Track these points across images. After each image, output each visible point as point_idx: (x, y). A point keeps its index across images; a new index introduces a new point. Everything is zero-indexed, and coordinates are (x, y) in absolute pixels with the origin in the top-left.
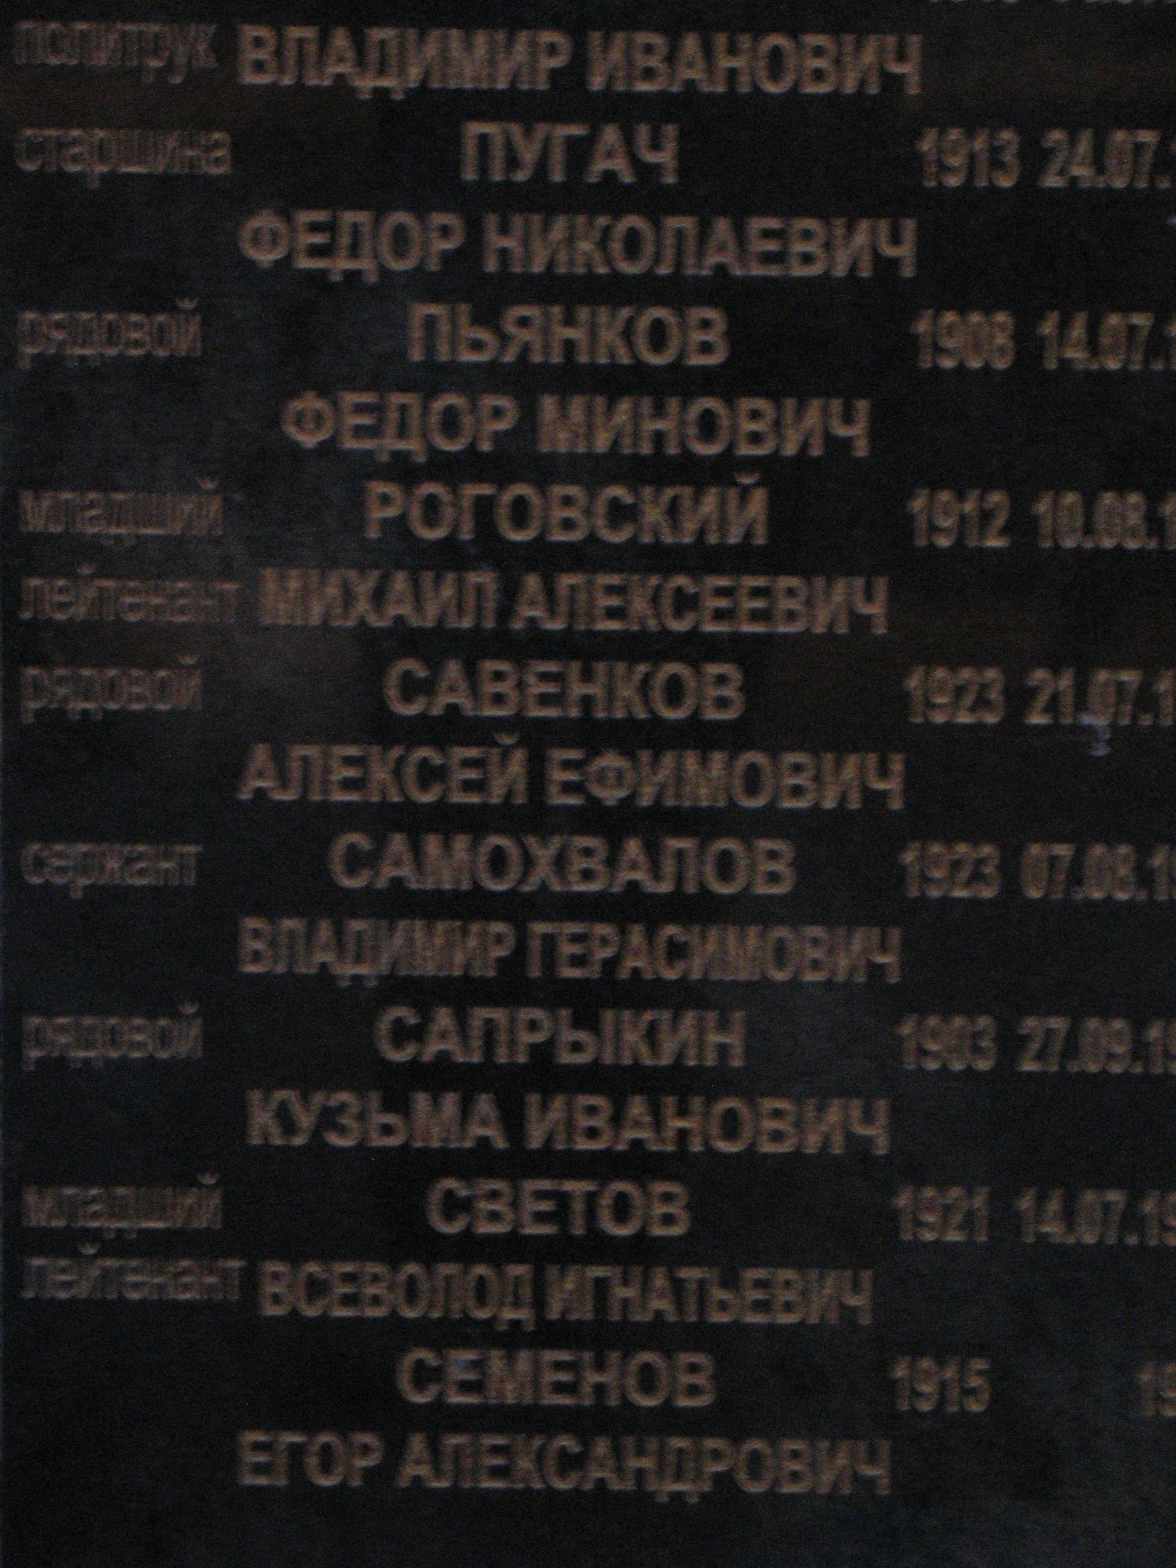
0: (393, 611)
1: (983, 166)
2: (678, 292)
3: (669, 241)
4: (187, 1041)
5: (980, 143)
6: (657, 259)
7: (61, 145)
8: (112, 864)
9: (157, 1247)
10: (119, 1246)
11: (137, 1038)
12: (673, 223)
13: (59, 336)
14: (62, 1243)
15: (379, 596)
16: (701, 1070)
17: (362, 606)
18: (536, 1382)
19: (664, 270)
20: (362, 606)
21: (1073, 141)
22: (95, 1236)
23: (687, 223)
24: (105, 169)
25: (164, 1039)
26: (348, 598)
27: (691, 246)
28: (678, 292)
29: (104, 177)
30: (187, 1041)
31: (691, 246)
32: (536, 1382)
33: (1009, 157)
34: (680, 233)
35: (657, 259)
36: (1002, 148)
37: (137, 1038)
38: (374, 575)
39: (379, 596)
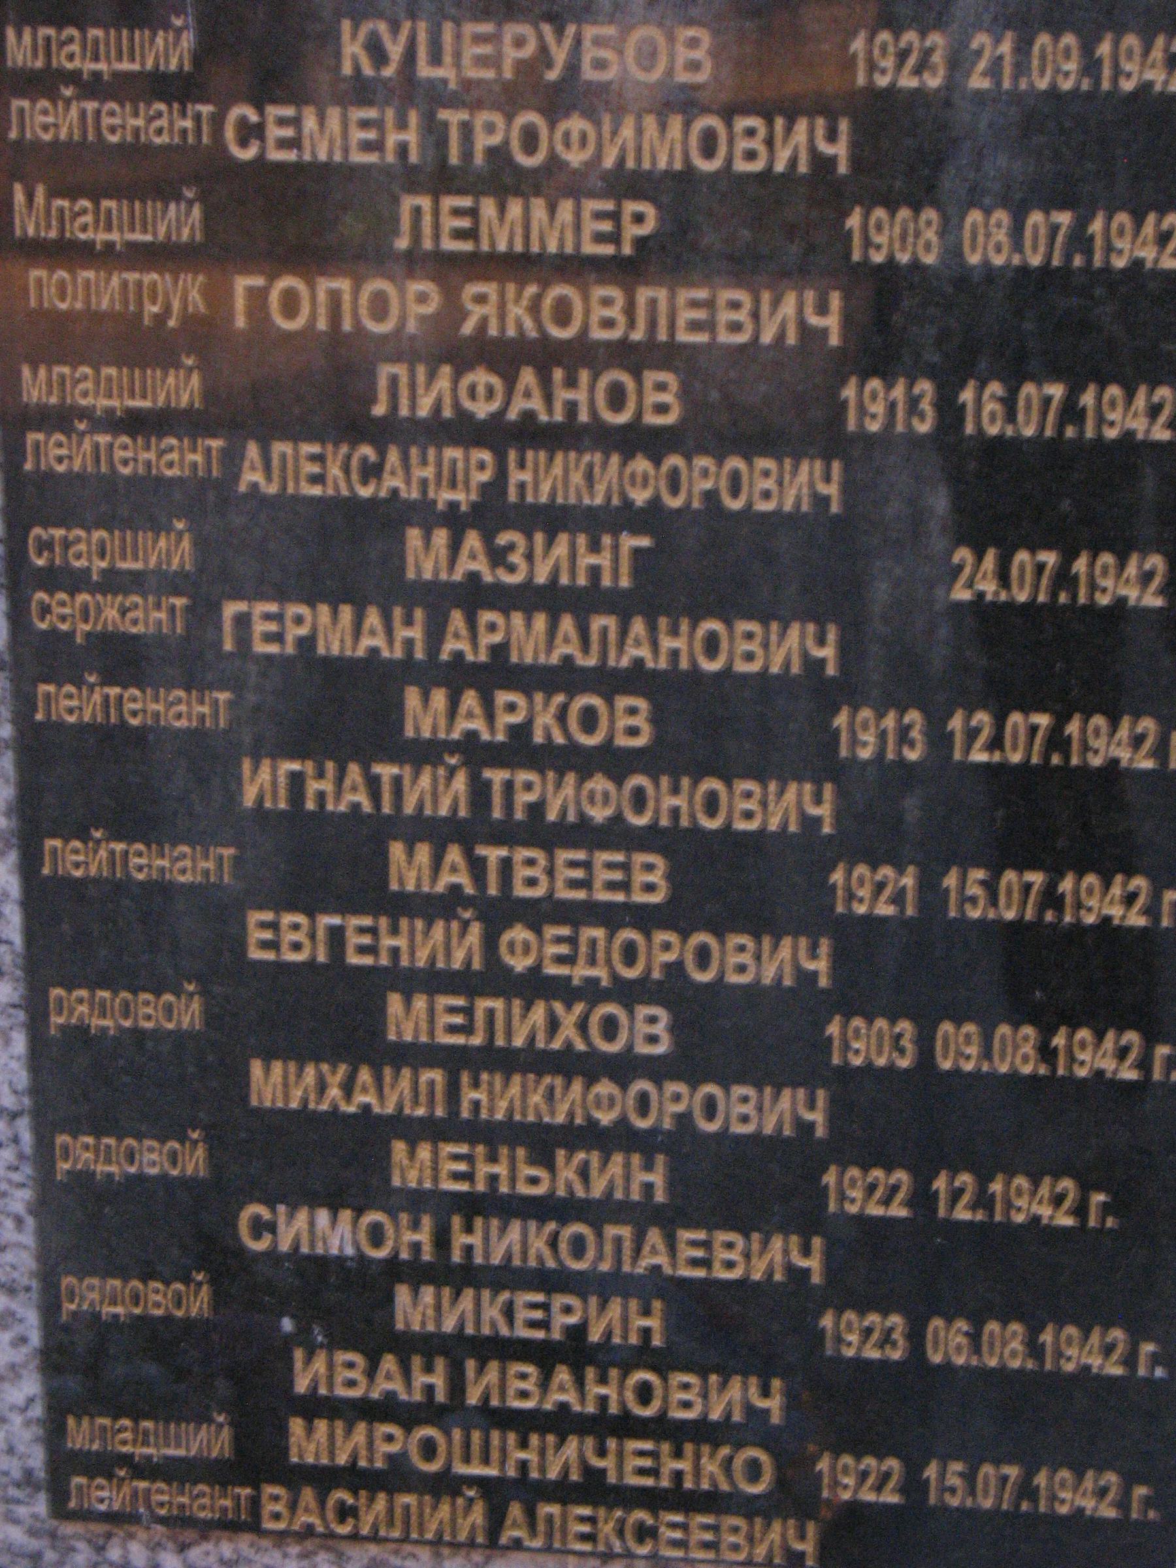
0: (361, 1098)
1: (900, 414)
2: (611, 683)
3: (608, 1248)
4: (194, 1161)
5: (898, 392)
6: (600, 1257)
7: (66, 544)
8: (111, 614)
9: (136, 424)
10: (93, 87)
11: (152, 1158)
12: (611, 1231)
13: (89, 1155)
14: (61, 419)
15: (348, 1088)
16: (572, 589)
17: (334, 1092)
18: (435, 1169)
19: (605, 1267)
20: (334, 1092)
21: (980, 557)
22: (73, 77)
23: (626, 1232)
24: (104, 565)
25: (173, 1158)
26: (322, 1087)
27: (627, 1252)
28: (611, 683)
29: (103, 572)
30: (188, 1013)
31: (627, 1252)
32: (435, 1169)
33: (926, 406)
34: (618, 1241)
35: (600, 1257)
36: (909, 727)
37: (152, 1158)
38: (343, 1069)
39: (348, 1088)
